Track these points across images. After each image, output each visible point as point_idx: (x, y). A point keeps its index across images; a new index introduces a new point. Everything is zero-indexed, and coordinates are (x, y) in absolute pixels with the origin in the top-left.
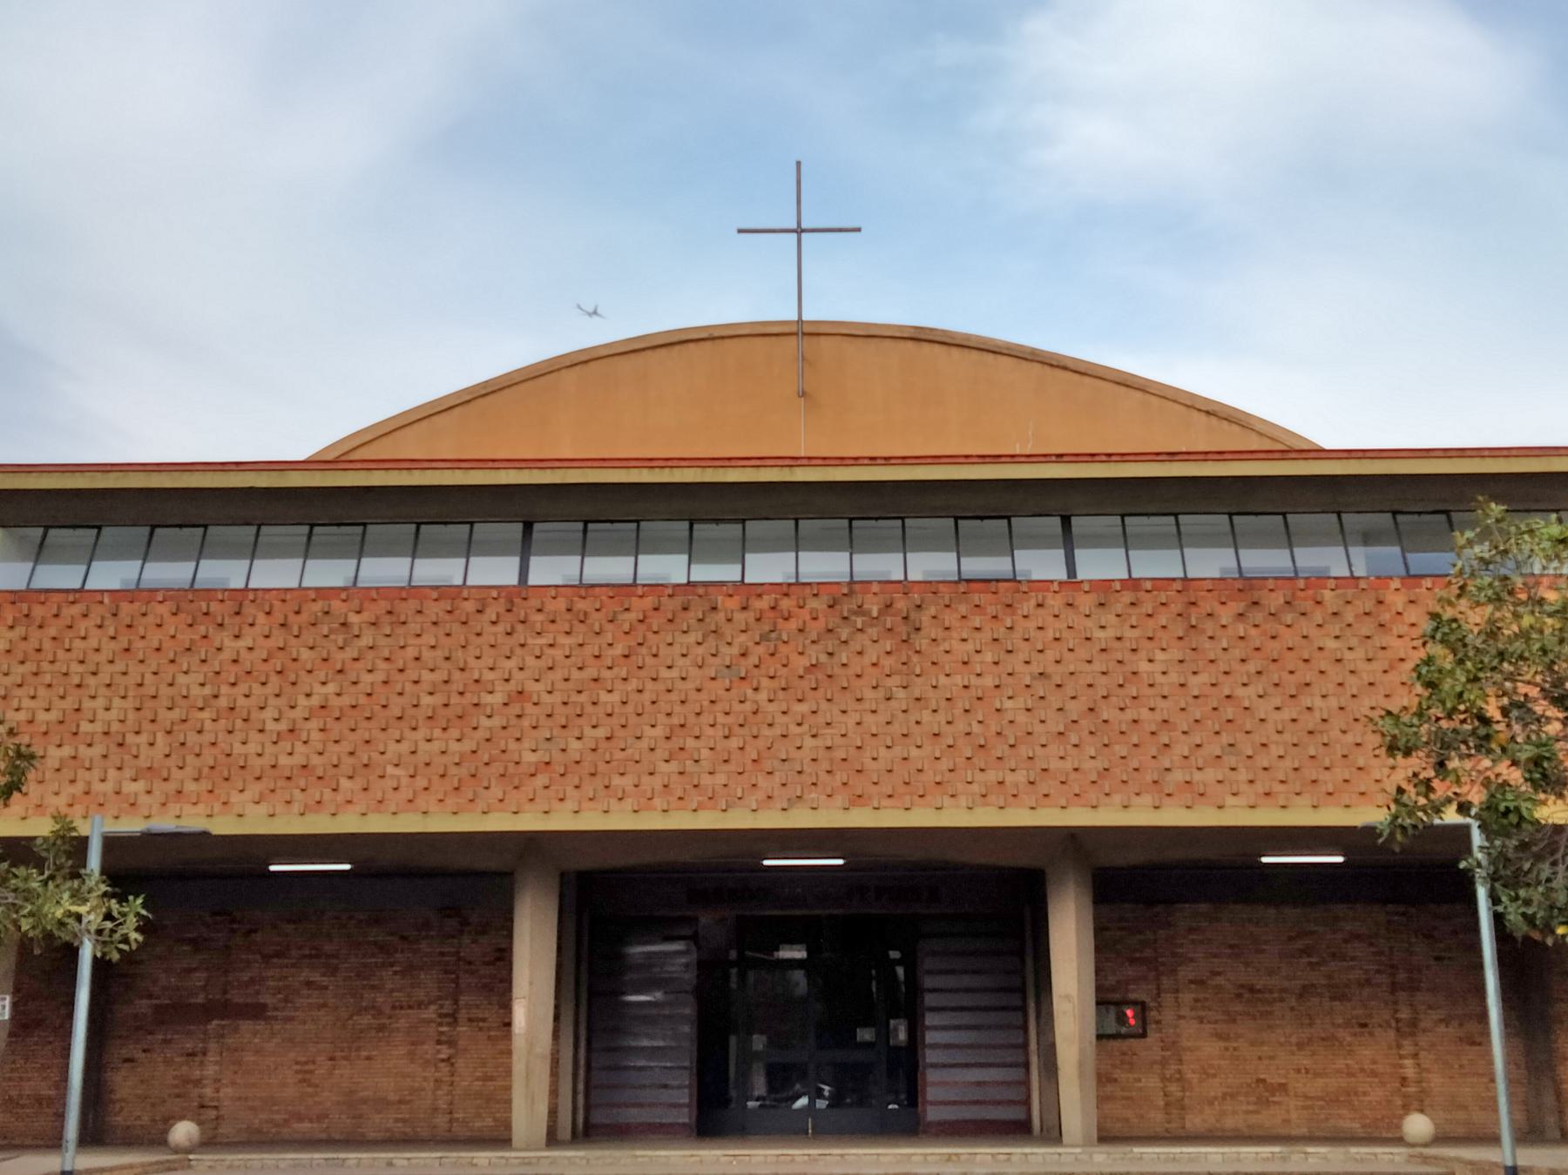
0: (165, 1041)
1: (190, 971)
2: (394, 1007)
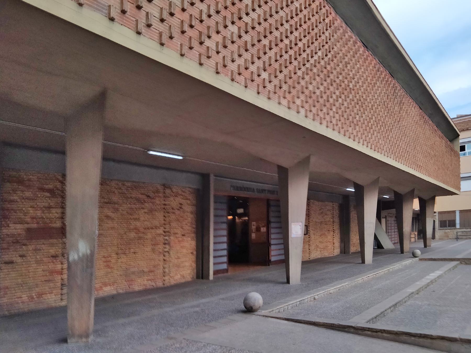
0: (36, 250)
1: (50, 207)
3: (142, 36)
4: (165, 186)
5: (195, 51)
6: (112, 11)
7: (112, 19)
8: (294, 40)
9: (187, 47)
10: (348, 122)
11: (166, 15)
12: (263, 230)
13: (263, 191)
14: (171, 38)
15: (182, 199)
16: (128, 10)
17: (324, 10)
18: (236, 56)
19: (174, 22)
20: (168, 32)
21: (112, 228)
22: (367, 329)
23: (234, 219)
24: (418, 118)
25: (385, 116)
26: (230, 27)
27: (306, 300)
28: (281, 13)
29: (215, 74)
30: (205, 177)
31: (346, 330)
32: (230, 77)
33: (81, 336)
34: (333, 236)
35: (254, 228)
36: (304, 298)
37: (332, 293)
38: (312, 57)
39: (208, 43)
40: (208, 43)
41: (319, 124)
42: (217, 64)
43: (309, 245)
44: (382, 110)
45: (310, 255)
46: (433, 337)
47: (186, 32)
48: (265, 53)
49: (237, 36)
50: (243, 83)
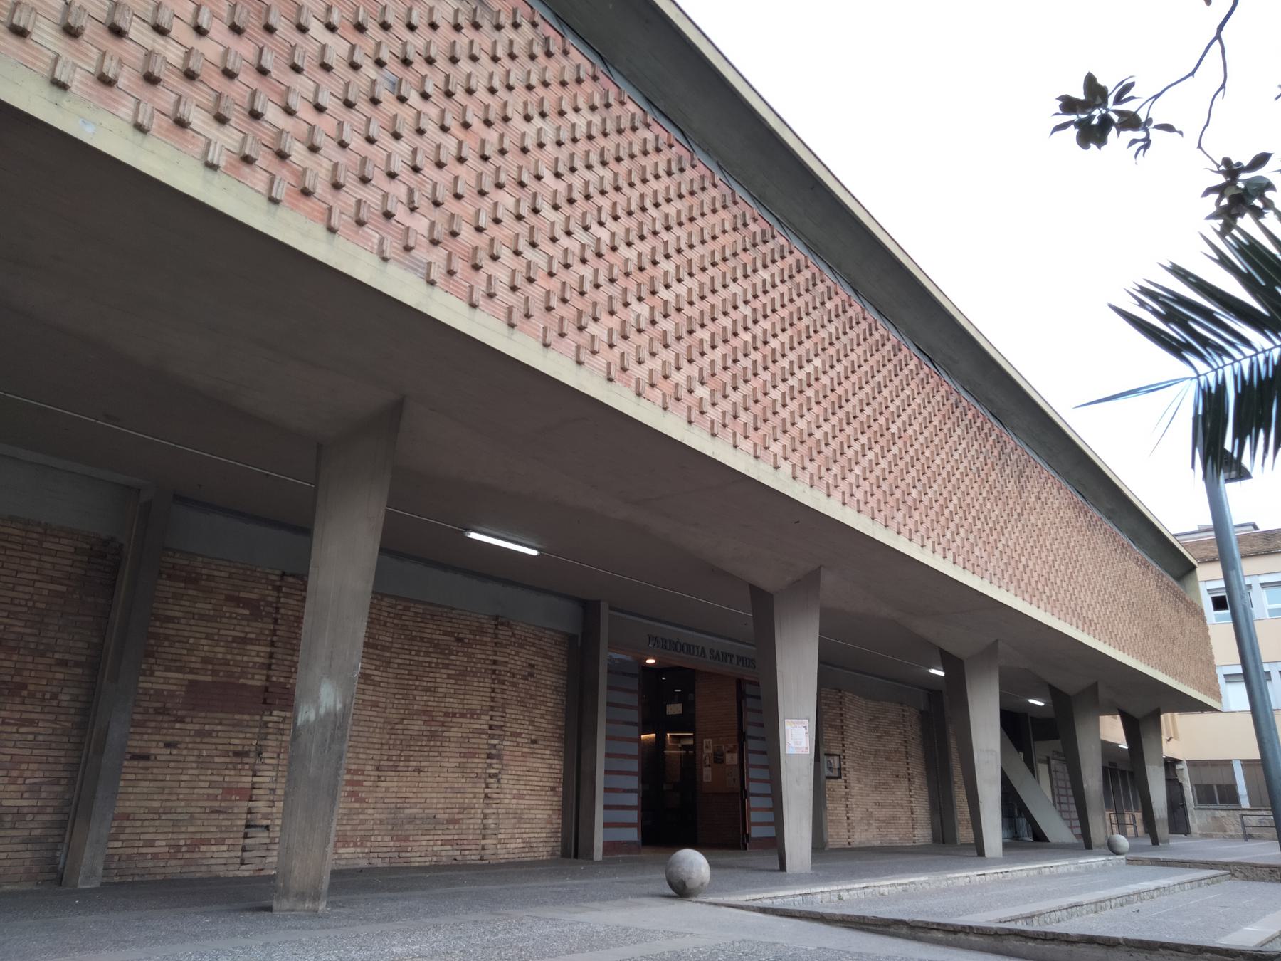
0: (201, 733)
1: (244, 641)
2: (446, 715)
3: (478, 310)
4: (498, 621)
5: (568, 341)
6: (432, 270)
7: (432, 283)
8: (761, 335)
9: (554, 333)
10: (892, 501)
11: (520, 281)
12: (732, 759)
13: (726, 656)
14: (528, 316)
15: (536, 654)
16: (459, 271)
17: (821, 287)
18: (645, 355)
19: (535, 292)
20: (523, 306)
21: (375, 705)
22: (935, 927)
23: (660, 739)
24: (1070, 513)
25: (984, 498)
26: (635, 305)
27: (819, 897)
28: (733, 288)
29: (605, 382)
30: (589, 609)
31: (891, 930)
32: (634, 389)
33: (302, 896)
34: (910, 791)
35: (708, 752)
36: (813, 890)
37: (887, 893)
38: (801, 367)
39: (592, 328)
40: (592, 328)
41: (825, 497)
42: (609, 364)
43: (847, 806)
44: (975, 485)
45: (851, 834)
46: (1070, 939)
47: (554, 308)
48: (703, 354)
49: (648, 322)
50: (660, 402)
